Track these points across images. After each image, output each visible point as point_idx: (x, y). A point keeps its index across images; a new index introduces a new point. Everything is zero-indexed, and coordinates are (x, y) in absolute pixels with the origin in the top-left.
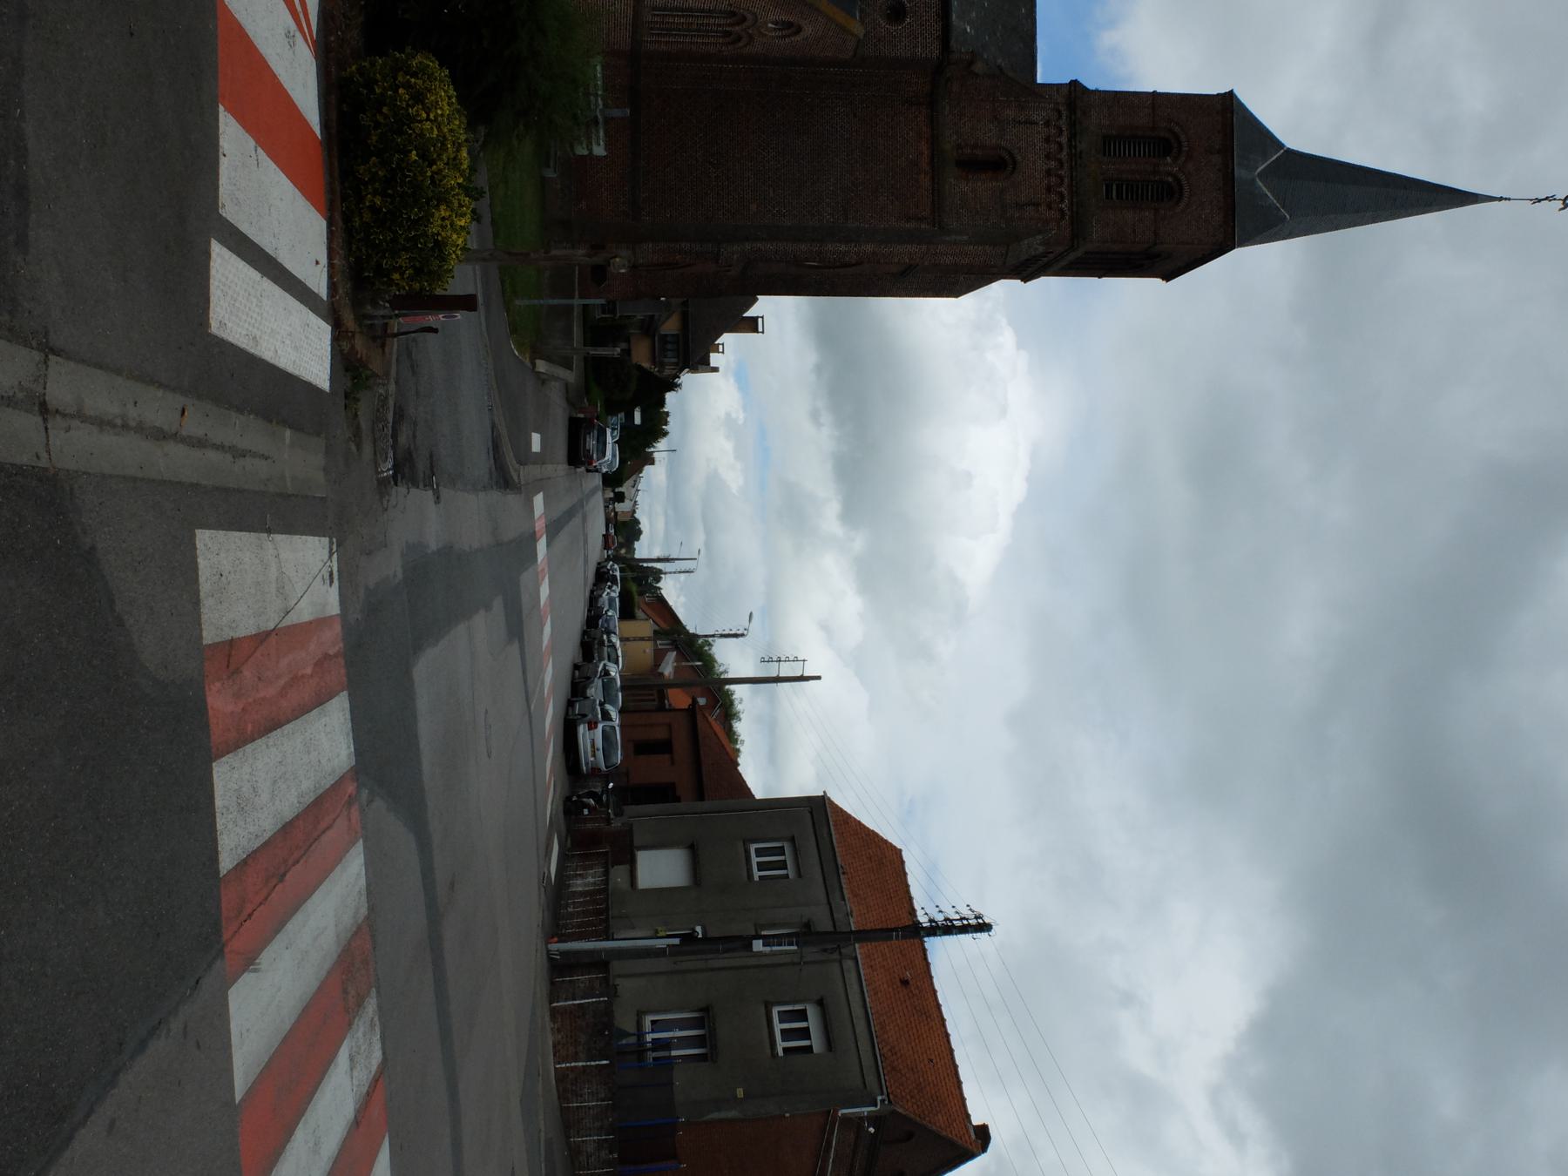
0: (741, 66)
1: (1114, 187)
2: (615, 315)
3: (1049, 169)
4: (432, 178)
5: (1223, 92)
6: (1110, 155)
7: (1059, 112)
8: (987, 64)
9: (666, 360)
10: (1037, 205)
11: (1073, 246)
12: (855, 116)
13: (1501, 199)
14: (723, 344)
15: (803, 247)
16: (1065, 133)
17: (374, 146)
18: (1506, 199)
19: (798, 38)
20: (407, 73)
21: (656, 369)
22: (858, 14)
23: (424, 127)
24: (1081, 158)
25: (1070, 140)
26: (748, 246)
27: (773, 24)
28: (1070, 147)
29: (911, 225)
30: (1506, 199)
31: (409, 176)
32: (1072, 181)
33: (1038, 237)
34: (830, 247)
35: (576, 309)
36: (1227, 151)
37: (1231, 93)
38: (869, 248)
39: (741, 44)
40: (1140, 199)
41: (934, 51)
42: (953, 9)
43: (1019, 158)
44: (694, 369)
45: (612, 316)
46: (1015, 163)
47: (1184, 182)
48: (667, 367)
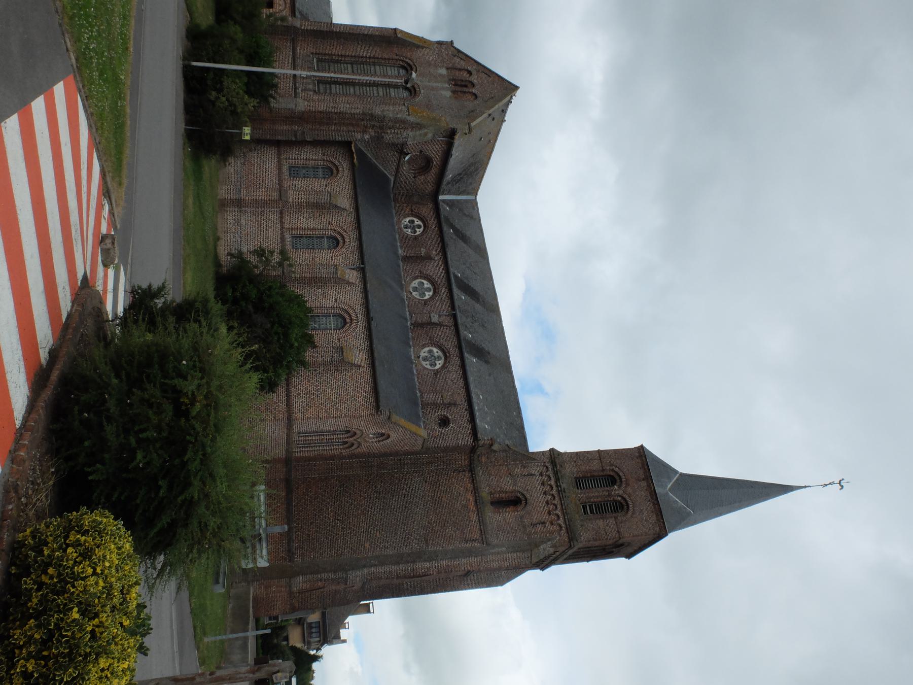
0: (354, 460)
1: (593, 505)
2: (278, 620)
3: (547, 501)
4: (93, 632)
5: (637, 446)
6: (581, 488)
7: (547, 468)
8: (500, 445)
9: (312, 640)
10: (544, 523)
11: (571, 546)
12: (426, 482)
13: (805, 487)
14: (348, 623)
15: (402, 567)
16: (553, 479)
17: (33, 609)
18: (808, 487)
19: (388, 441)
20: (78, 532)
21: (306, 647)
22: (422, 424)
23: (88, 583)
24: (564, 492)
25: (556, 482)
26: (366, 571)
27: (372, 434)
28: (557, 486)
29: (469, 545)
30: (808, 487)
31: (66, 636)
32: (562, 506)
33: (548, 543)
34: (419, 565)
35: (250, 638)
36: (648, 478)
37: (642, 446)
38: (444, 563)
39: (353, 448)
40: (607, 512)
41: (469, 441)
42: (477, 417)
43: (528, 496)
44: (330, 643)
45: (275, 621)
46: (526, 499)
47: (628, 499)
48: (313, 644)
